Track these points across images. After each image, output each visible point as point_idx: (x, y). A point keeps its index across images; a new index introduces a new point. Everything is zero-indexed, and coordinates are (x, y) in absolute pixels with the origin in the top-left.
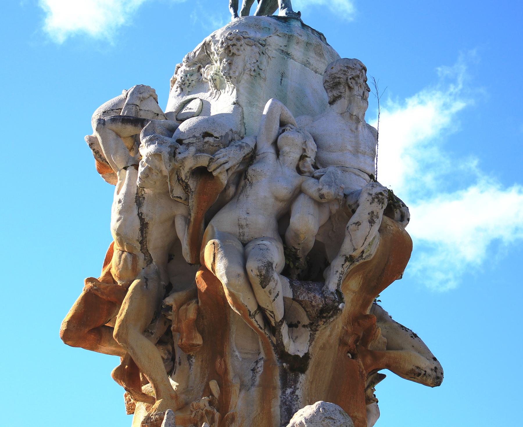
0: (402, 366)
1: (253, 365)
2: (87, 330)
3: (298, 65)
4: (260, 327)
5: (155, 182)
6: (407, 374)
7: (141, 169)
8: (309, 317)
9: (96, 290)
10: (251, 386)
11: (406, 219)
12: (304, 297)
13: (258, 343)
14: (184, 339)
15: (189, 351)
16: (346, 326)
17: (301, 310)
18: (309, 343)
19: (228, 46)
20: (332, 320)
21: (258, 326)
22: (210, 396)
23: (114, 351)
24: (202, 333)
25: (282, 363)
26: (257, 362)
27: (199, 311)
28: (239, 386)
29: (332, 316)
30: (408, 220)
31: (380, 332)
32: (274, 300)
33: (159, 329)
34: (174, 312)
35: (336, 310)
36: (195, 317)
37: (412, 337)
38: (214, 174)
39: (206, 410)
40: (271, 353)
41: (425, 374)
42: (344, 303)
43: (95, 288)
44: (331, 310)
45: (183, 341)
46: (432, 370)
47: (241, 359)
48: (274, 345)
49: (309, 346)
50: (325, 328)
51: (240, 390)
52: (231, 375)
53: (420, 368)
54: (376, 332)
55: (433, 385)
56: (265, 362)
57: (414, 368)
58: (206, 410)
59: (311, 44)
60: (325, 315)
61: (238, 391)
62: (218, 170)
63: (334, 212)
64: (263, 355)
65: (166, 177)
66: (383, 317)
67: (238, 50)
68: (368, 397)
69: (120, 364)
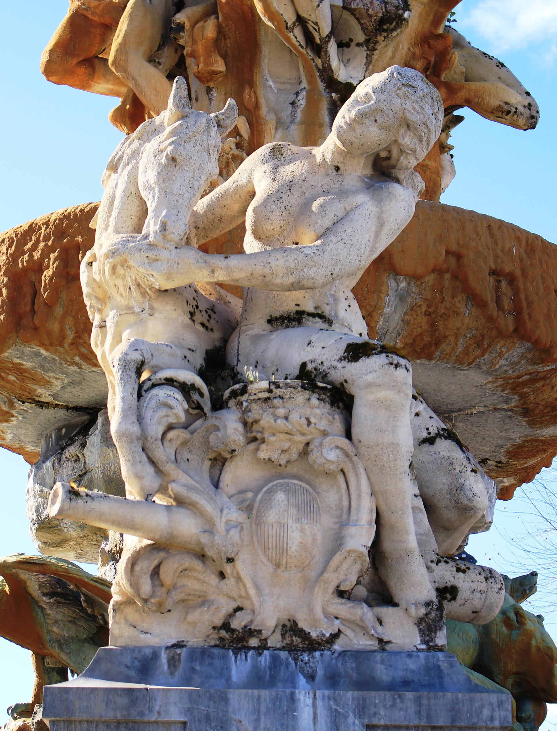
0: (485, 101)
1: (292, 97)
2: (75, 61)
4: (300, 45)
6: (492, 113)
8: (364, 31)
9: (85, 9)
10: (291, 123)
12: (358, 5)
13: (298, 70)
14: (201, 65)
15: (208, 81)
16: (413, 47)
17: (353, 22)
18: (365, 67)
20: (394, 34)
21: (297, 44)
22: (238, 137)
23: (112, 90)
24: (224, 57)
25: (330, 92)
26: (297, 94)
27: (219, 29)
28: (274, 123)
29: (395, 29)
31: (457, 58)
32: (319, 6)
33: (168, 57)
34: (187, 31)
35: (400, 21)
36: (215, 36)
37: (498, 66)
39: (233, 154)
40: (316, 81)
41: (516, 112)
42: (410, 11)
43: (83, 7)
44: (393, 20)
45: (200, 68)
46: (525, 107)
47: (276, 91)
48: (319, 71)
49: (366, 71)
50: (386, 46)
51: (276, 129)
52: (264, 111)
53: (509, 104)
54: (451, 58)
55: (526, 127)
56: (307, 93)
57: (502, 104)
58: (233, 154)
60: (385, 27)
61: (273, 130)
64: (304, 84)
66: (459, 43)
68: (442, 144)
69: (120, 104)
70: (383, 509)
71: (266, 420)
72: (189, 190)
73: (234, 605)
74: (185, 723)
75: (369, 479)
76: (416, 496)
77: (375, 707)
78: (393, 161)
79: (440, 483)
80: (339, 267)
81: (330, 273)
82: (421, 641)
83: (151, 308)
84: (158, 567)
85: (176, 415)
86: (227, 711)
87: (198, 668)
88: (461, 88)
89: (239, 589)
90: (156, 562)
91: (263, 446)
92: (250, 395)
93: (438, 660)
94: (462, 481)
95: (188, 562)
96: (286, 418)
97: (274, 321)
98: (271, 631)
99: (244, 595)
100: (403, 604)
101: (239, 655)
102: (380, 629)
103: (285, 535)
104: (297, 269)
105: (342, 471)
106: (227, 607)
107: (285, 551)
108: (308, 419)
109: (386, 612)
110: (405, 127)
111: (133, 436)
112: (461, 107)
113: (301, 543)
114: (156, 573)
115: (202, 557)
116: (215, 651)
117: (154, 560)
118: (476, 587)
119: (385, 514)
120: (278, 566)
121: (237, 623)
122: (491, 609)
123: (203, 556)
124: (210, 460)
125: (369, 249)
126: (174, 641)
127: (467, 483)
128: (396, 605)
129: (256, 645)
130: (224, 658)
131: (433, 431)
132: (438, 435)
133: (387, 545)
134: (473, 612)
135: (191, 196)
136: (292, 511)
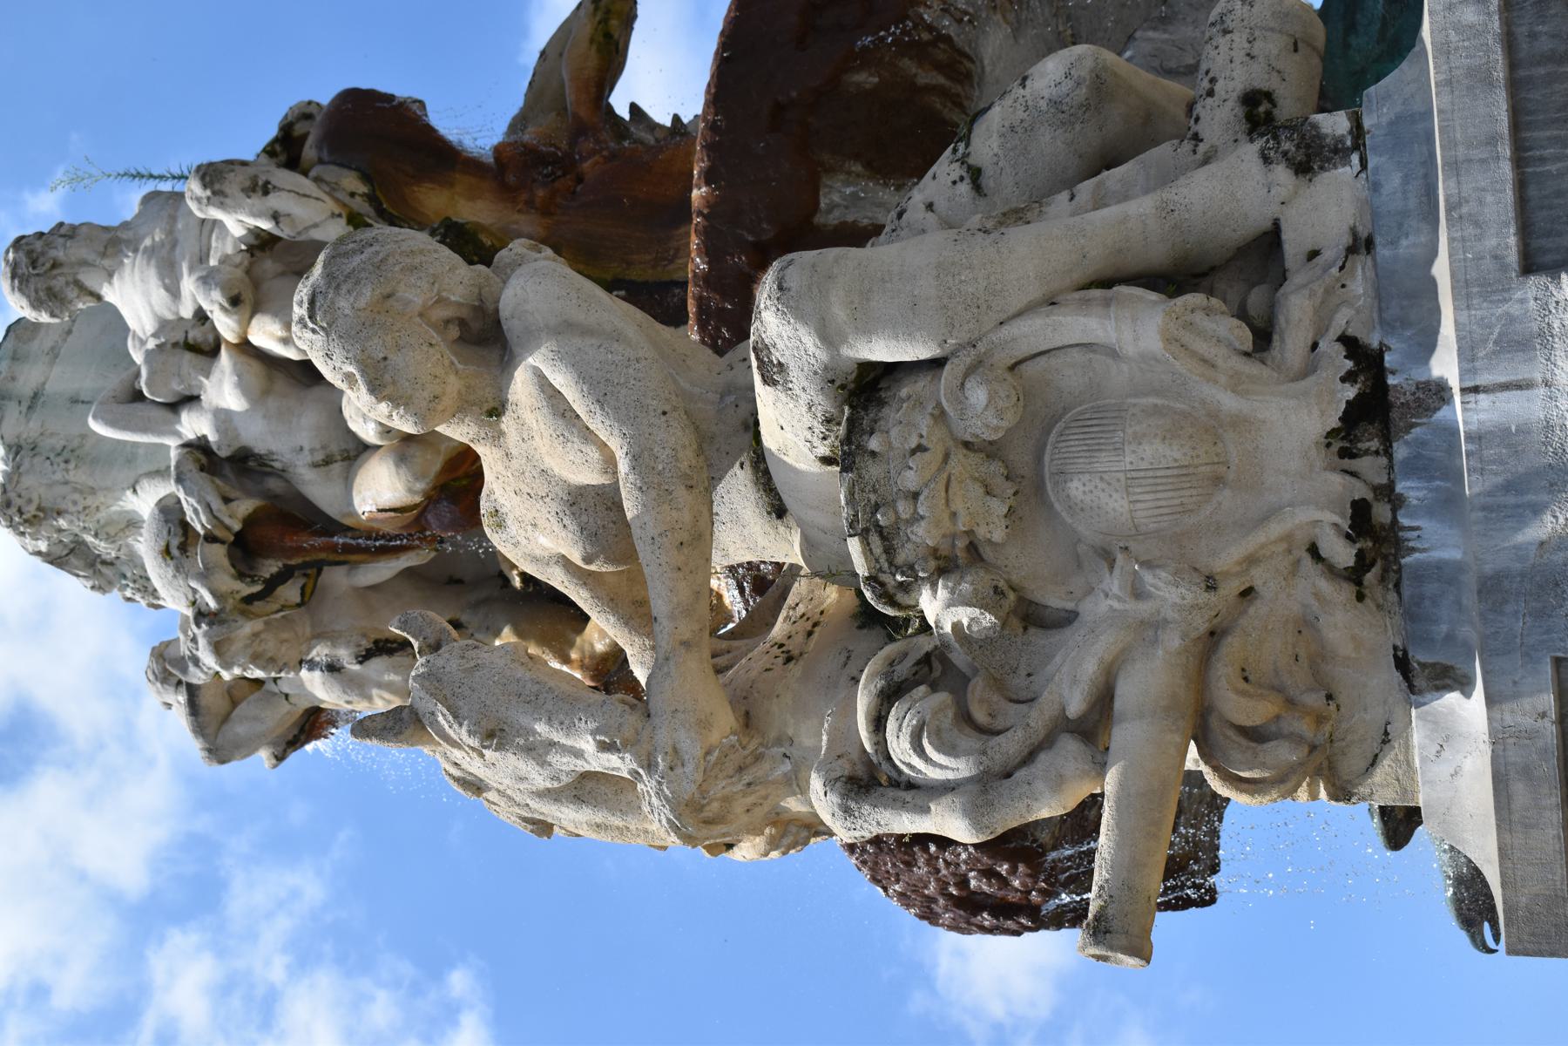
3: (57, 370)
5: (282, 642)
7: (258, 674)
11: (308, 110)
19: (26, 521)
30: (310, 103)
38: (237, 527)
59: (15, 352)
62: (227, 521)
63: (279, 267)
65: (266, 623)
67: (30, 501)
70: (1078, 276)
71: (924, 535)
72: (541, 701)
73: (1307, 560)
74: (1558, 662)
75: (1019, 314)
76: (1072, 198)
77: (1482, 258)
79: (1051, 144)
80: (649, 401)
81: (663, 418)
82: (1344, 165)
83: (779, 741)
84: (1244, 731)
86: (1523, 575)
87: (1444, 628)
89: (1271, 557)
91: (982, 532)
92: (880, 570)
93: (1377, 126)
94: (1043, 104)
95: (1224, 673)
96: (915, 496)
98: (1353, 480)
99: (1284, 546)
100: (1272, 210)
101: (1411, 544)
103: (1151, 474)
104: (660, 485)
105: (1012, 368)
107: (1184, 471)
108: (913, 452)
109: (1293, 244)
110: (391, 301)
111: (979, 802)
112: (610, 109)
113: (1164, 438)
114: (1255, 735)
115: (1214, 636)
116: (1407, 591)
117: (1227, 737)
118: (1243, 53)
119: (1091, 269)
120: (1218, 481)
121: (1343, 554)
122: (1287, 15)
123: (1212, 634)
124: (1025, 629)
125: (616, 345)
126: (1397, 676)
128: (1276, 224)
129: (1388, 507)
132: (963, 161)
133: (1157, 254)
134: (1296, 50)
135: (550, 696)
136: (1104, 461)
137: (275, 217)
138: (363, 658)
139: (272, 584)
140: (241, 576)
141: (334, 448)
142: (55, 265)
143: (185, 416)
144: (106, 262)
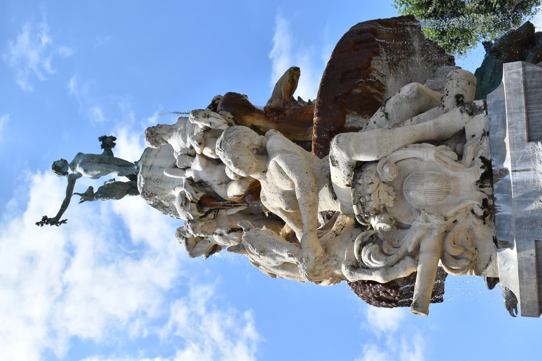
7: (203, 236)
62: (196, 198)
70: (413, 140)
73: (471, 213)
78: (258, 147)
79: (406, 107)
83: (334, 256)
85: (375, 249)
86: (527, 219)
87: (506, 232)
88: (285, 100)
90: (450, 257)
91: (387, 204)
93: (491, 104)
94: (404, 97)
96: (370, 195)
97: (471, 106)
100: (463, 125)
102: (477, 136)
105: (396, 163)
106: (472, 219)
108: (370, 184)
109: (468, 133)
112: (293, 98)
114: (456, 258)
115: (446, 232)
116: (496, 222)
119: (416, 139)
120: (448, 193)
123: (446, 232)
126: (494, 244)
127: (405, 95)
130: (500, 218)
131: (382, 114)
133: (433, 135)
137: (210, 123)
138: (229, 232)
139: (207, 214)
140: (199, 211)
141: (223, 180)
142: (157, 134)
143: (187, 172)
144: (169, 134)
